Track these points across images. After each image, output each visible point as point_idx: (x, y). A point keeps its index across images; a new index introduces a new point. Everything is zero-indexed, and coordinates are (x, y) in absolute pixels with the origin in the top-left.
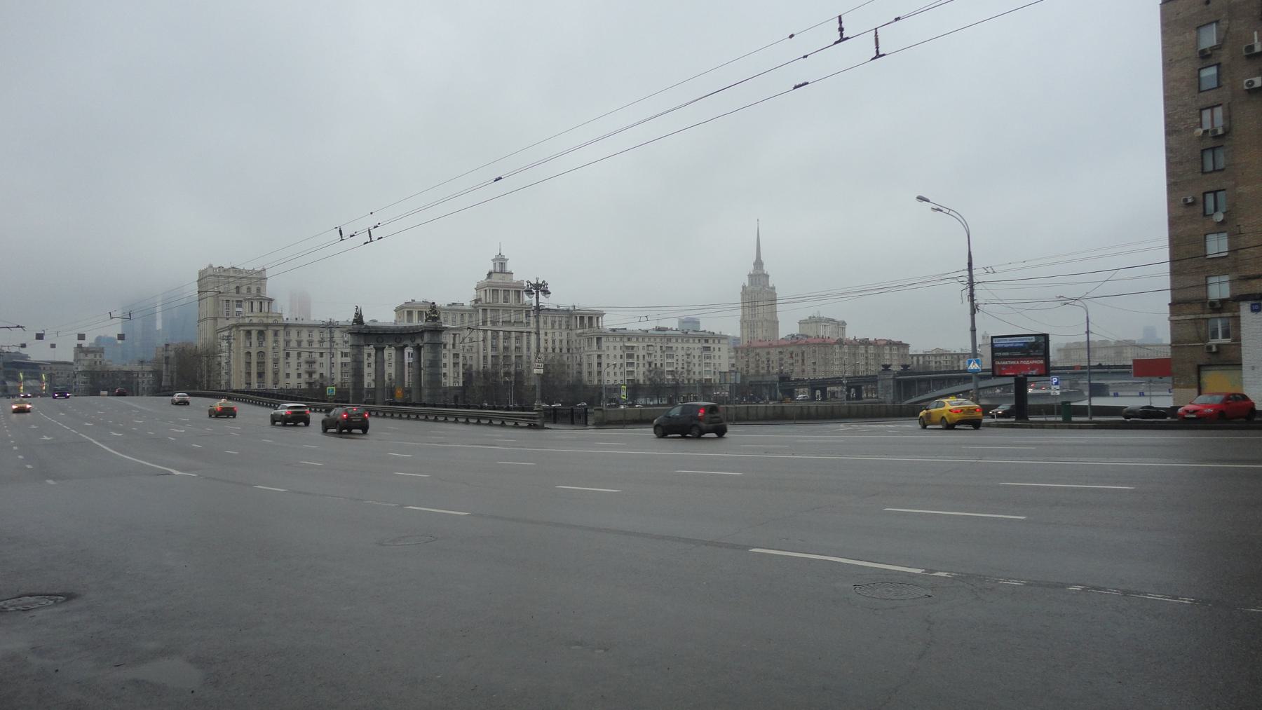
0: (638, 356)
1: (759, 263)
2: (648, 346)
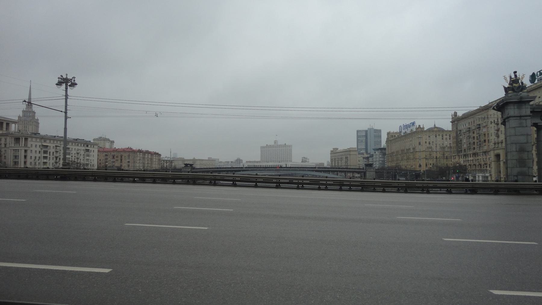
0: (50, 152)
2: (56, 146)
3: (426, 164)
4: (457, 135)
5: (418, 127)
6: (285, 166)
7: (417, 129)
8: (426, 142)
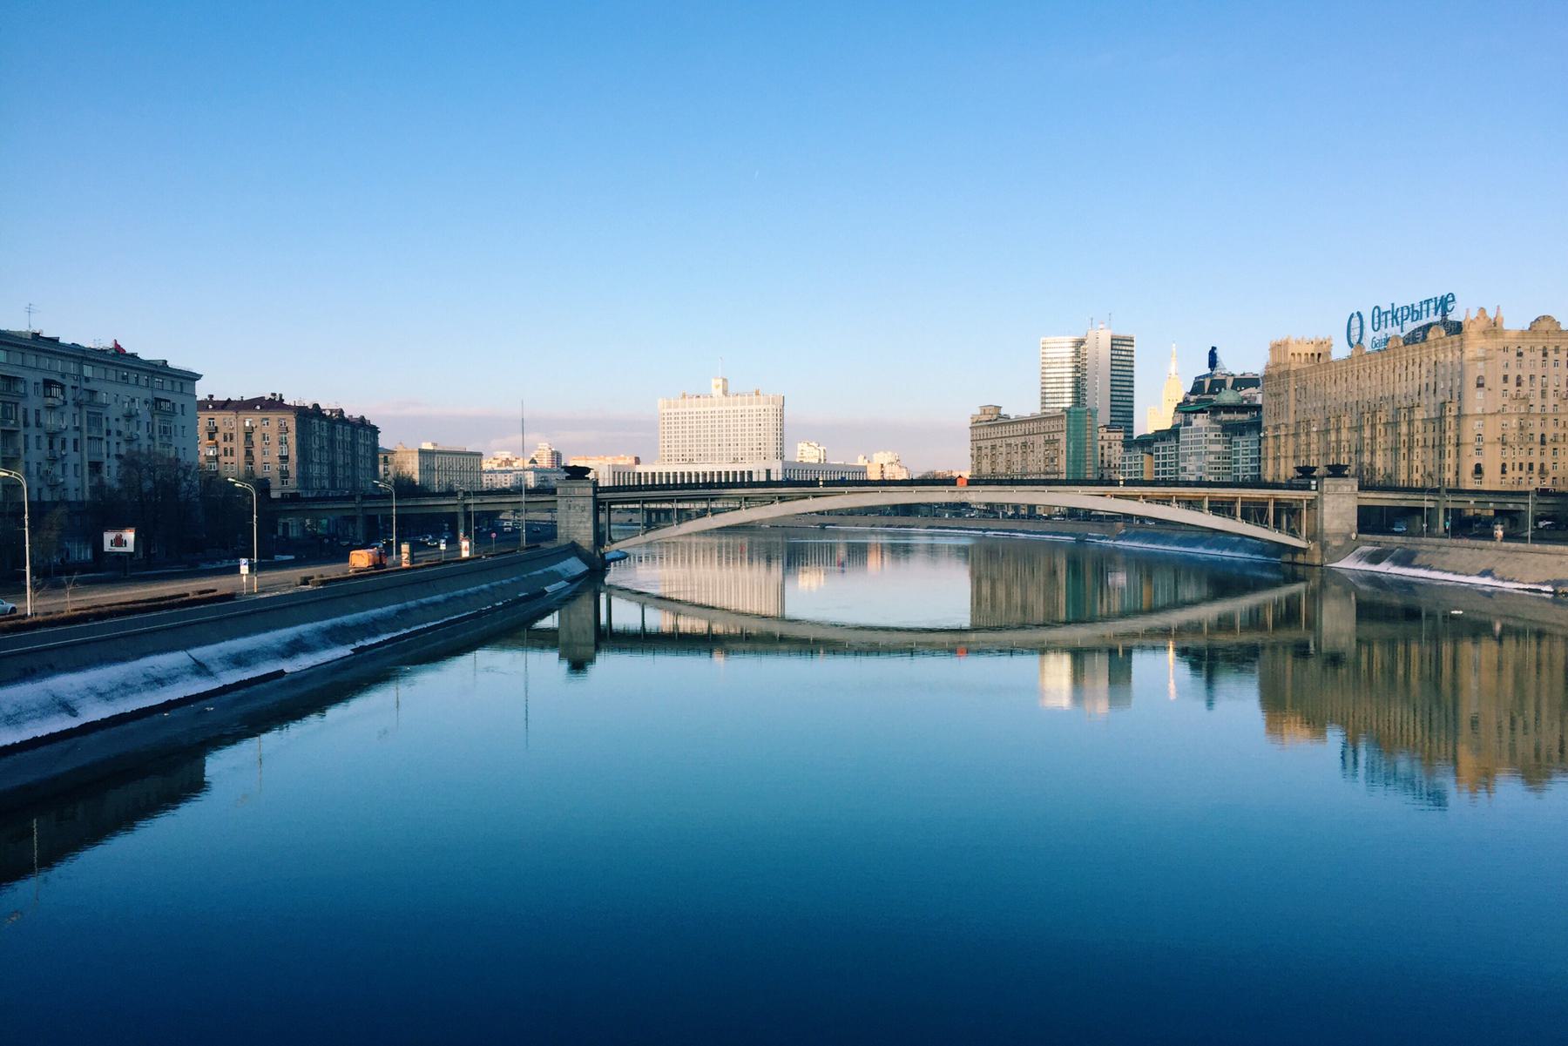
3: (1504, 465)
6: (763, 478)
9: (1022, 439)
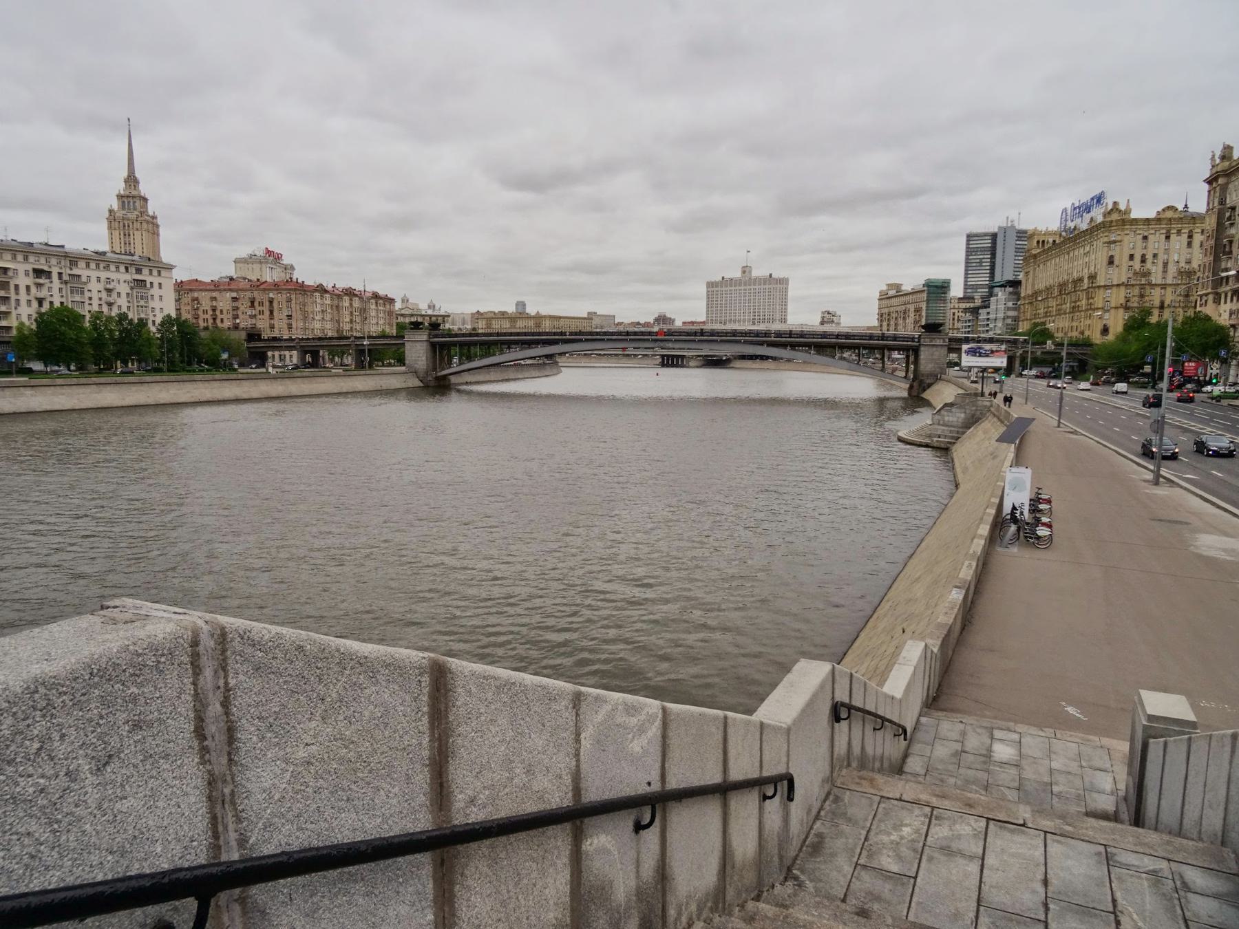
0: (17, 287)
1: (132, 180)
4: (1220, 225)
5: (1110, 207)
7: (1107, 214)
8: (1131, 257)
9: (903, 307)
